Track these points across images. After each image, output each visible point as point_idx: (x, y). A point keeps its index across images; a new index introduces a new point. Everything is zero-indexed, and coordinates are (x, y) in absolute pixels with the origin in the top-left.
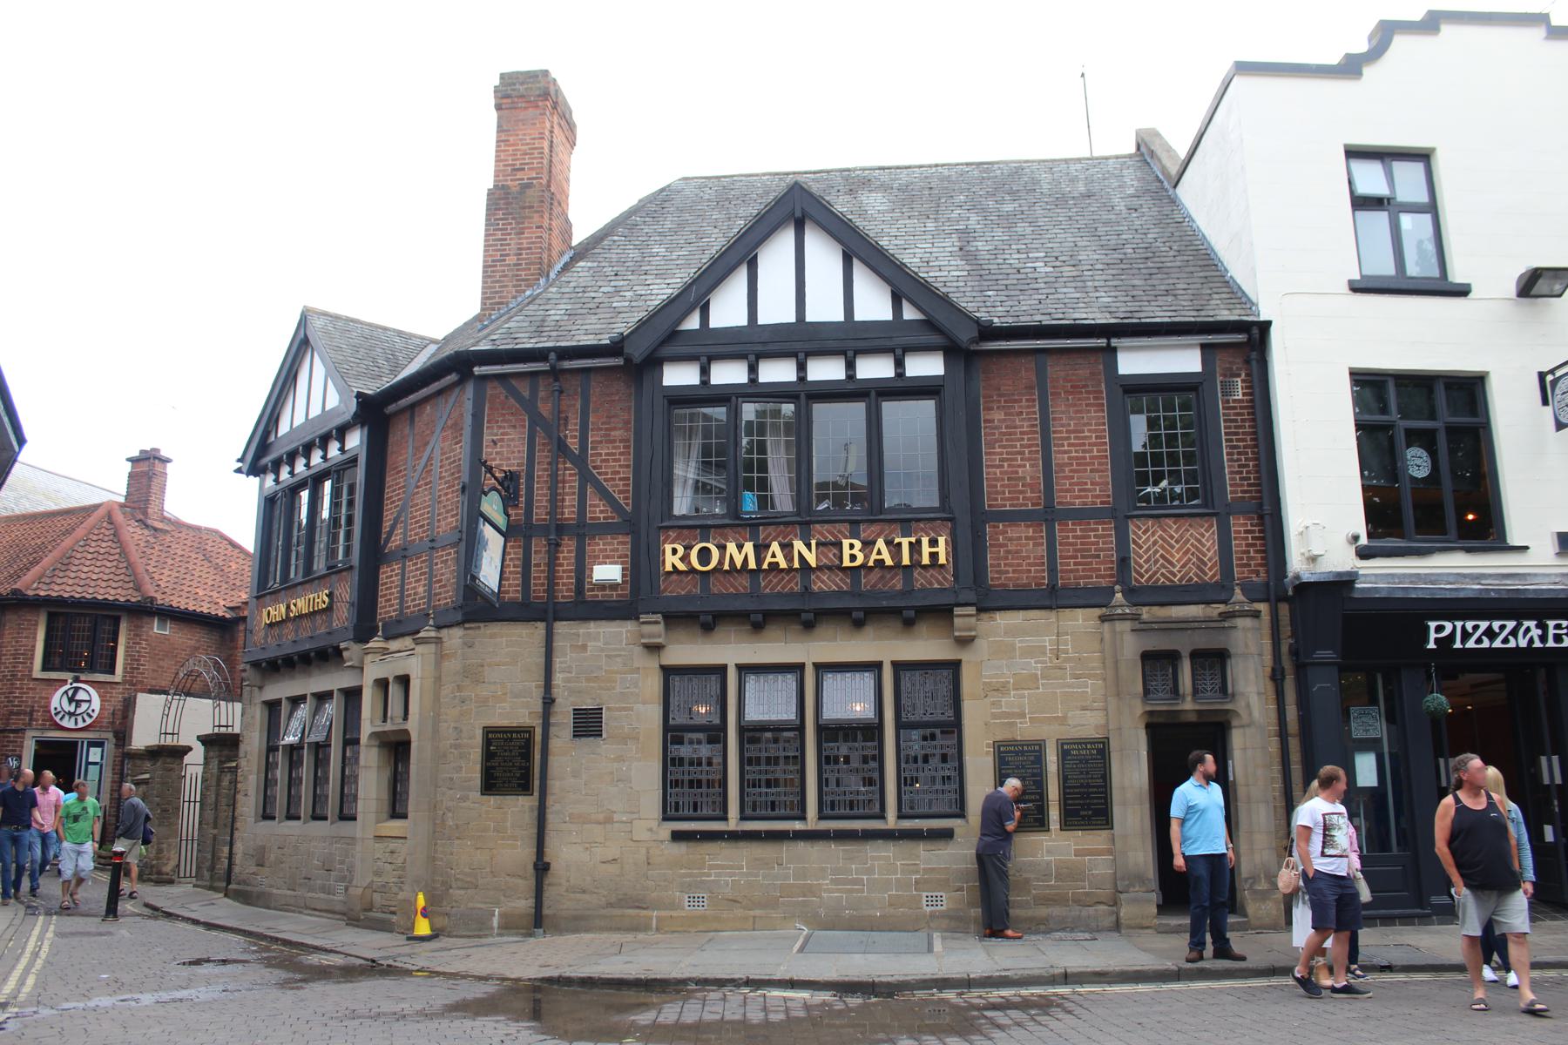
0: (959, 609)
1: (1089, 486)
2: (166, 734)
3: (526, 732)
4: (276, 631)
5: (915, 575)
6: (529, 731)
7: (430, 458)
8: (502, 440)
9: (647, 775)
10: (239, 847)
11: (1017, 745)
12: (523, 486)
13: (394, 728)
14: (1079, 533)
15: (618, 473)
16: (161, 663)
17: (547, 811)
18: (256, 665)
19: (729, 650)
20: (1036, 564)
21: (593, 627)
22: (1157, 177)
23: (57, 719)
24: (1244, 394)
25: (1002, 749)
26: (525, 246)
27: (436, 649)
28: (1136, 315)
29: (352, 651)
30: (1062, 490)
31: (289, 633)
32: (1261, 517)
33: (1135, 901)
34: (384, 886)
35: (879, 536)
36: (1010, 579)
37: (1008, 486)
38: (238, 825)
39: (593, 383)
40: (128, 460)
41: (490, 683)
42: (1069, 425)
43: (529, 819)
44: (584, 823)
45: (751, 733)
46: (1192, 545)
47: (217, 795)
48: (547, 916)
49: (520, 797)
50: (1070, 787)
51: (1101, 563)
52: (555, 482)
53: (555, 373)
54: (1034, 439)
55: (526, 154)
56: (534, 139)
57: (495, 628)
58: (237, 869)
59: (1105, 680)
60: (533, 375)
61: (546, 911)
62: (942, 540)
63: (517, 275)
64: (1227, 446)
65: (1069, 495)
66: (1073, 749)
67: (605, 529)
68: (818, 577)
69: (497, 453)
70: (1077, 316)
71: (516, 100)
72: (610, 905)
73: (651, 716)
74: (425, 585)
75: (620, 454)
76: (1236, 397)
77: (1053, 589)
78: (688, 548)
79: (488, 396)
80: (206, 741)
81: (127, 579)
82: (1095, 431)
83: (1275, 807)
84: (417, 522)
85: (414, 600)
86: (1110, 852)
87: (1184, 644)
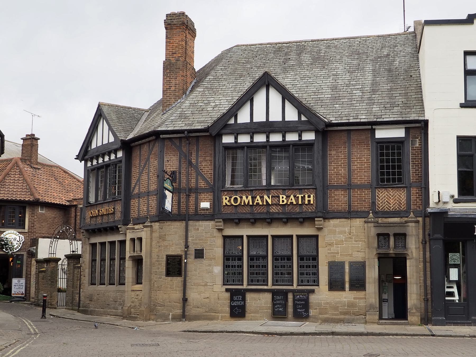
0: (317, 218)
2: (51, 254)
3: (180, 256)
4: (94, 219)
6: (181, 256)
9: (218, 270)
11: (336, 263)
14: (359, 193)
17: (187, 282)
18: (87, 231)
20: (344, 203)
21: (201, 223)
24: (419, 145)
25: (331, 264)
27: (151, 229)
29: (122, 228)
31: (99, 220)
33: (370, 314)
34: (135, 306)
36: (335, 208)
37: (336, 177)
40: (22, 139)
41: (168, 241)
42: (358, 156)
44: (198, 286)
51: (366, 203)
52: (188, 174)
53: (187, 138)
55: (176, 47)
56: (179, 41)
57: (169, 223)
58: (81, 302)
60: (180, 138)
61: (186, 314)
63: (175, 94)
65: (356, 180)
67: (204, 191)
69: (169, 164)
72: (206, 312)
73: (219, 252)
74: (146, 207)
75: (209, 165)
77: (349, 212)
78: (230, 198)
80: (68, 257)
81: (27, 191)
82: (366, 158)
84: (143, 186)
87: (391, 231)
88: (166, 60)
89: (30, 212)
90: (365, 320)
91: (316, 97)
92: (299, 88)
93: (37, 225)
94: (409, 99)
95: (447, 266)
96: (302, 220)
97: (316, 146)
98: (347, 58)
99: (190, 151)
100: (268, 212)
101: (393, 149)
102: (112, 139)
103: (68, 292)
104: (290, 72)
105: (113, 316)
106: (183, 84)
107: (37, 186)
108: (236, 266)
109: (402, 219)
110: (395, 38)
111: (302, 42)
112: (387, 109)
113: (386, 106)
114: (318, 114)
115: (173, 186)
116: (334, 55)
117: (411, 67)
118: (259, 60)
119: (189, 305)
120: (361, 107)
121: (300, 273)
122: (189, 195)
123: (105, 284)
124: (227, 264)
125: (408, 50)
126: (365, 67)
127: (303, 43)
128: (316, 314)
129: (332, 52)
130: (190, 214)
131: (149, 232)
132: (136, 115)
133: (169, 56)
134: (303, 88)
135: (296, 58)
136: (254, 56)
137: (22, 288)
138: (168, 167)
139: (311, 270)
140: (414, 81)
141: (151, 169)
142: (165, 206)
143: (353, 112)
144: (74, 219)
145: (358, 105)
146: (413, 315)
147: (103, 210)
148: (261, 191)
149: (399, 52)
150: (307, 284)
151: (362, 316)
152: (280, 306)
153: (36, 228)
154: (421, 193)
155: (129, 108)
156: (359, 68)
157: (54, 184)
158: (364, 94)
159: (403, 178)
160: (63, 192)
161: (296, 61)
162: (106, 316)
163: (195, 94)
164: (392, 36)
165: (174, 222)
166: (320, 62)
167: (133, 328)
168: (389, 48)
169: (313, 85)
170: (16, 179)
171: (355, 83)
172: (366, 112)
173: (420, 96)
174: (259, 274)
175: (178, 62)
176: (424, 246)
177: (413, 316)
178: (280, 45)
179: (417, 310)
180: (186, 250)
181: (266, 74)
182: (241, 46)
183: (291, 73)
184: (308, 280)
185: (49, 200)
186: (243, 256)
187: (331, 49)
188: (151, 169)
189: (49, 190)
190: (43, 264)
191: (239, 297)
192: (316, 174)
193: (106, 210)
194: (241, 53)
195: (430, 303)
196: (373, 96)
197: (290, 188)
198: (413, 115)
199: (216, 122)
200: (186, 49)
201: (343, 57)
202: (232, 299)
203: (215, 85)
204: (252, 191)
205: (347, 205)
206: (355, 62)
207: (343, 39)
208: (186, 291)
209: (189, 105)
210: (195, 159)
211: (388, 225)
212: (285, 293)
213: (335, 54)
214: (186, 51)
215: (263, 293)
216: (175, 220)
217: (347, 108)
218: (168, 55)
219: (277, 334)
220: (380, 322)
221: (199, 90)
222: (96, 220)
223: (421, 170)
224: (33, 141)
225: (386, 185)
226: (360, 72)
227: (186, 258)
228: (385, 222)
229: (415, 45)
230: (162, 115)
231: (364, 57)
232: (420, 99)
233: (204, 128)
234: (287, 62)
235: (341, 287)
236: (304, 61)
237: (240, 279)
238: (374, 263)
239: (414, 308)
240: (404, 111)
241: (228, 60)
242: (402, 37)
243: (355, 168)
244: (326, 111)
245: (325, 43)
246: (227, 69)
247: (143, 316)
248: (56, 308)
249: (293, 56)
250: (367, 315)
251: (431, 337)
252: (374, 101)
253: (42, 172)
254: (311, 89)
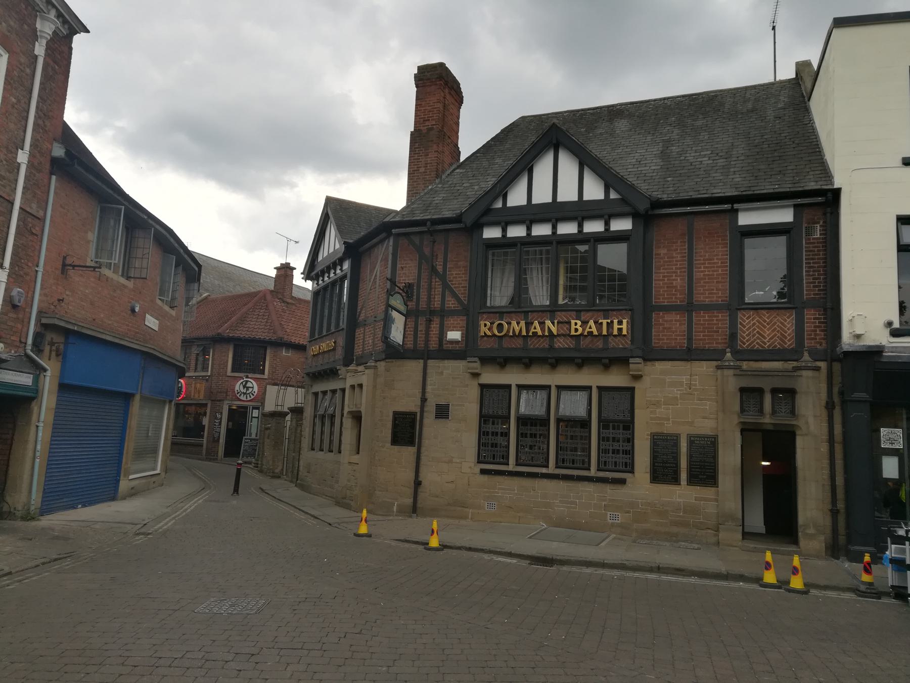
2: (281, 406)
3: (413, 415)
5: (610, 340)
6: (415, 414)
7: (376, 276)
8: (406, 267)
9: (470, 439)
10: (301, 463)
12: (415, 291)
14: (707, 318)
17: (422, 455)
19: (512, 377)
22: (803, 93)
23: (238, 395)
24: (820, 235)
26: (429, 162)
28: (753, 189)
29: (342, 370)
30: (698, 294)
32: (825, 310)
38: (301, 452)
40: (275, 268)
43: (413, 459)
45: (523, 421)
46: (778, 326)
47: (295, 437)
49: (409, 447)
50: (694, 462)
53: (431, 233)
55: (430, 111)
56: (434, 103)
58: (300, 473)
59: (717, 402)
61: (419, 505)
62: (625, 321)
63: (425, 178)
64: (806, 267)
65: (702, 296)
66: (697, 440)
67: (453, 313)
68: (558, 340)
70: (715, 191)
71: (425, 81)
73: (472, 410)
75: (463, 274)
77: (689, 349)
78: (492, 323)
83: (823, 485)
84: (370, 307)
85: (368, 346)
86: (716, 500)
87: (767, 384)
91: (636, 170)
133: (419, 124)
142: (391, 335)
146: (811, 537)
151: (709, 531)
170: (261, 314)
200: (444, 114)
210: (441, 265)
214: (444, 117)
237: (505, 454)
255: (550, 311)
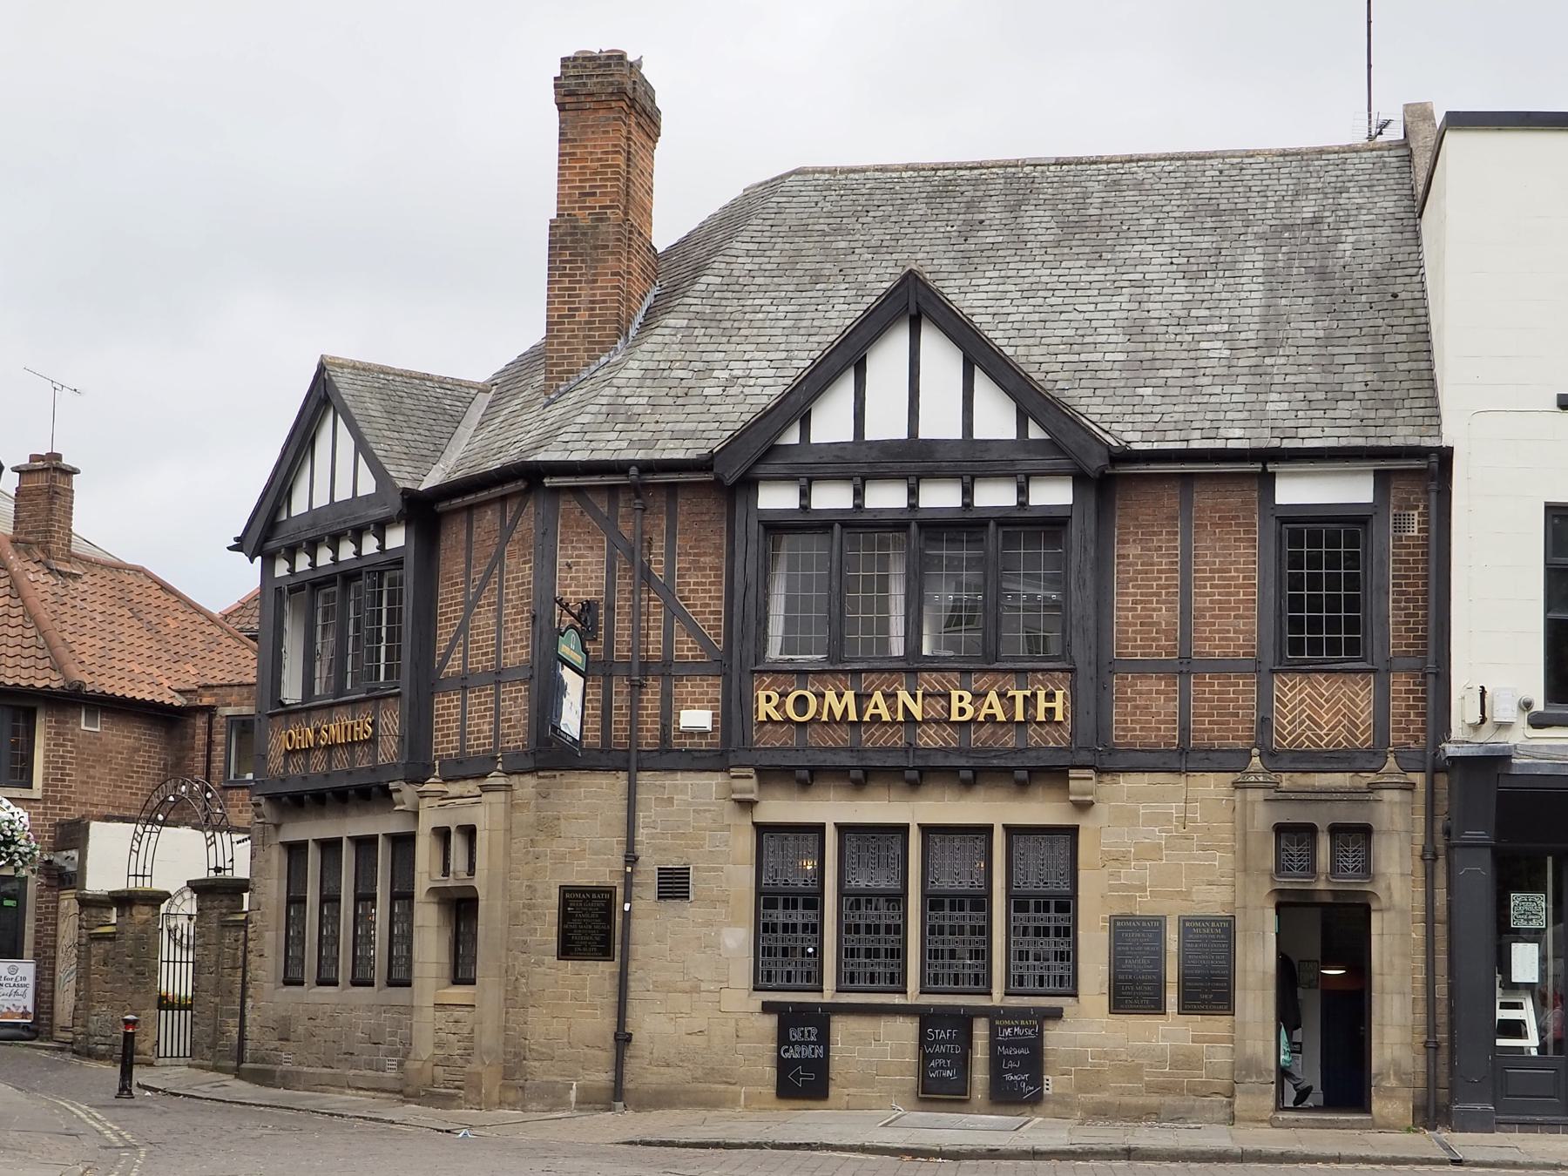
1: (1232, 635)
2: (136, 875)
6: (610, 891)
8: (577, 564)
9: (738, 939)
11: (1135, 921)
13: (458, 884)
14: (1216, 688)
15: (708, 605)
16: (92, 771)
17: (629, 977)
18: (273, 798)
20: (1165, 722)
21: (680, 779)
24: (1420, 530)
25: (1118, 924)
27: (506, 797)
29: (406, 793)
33: (1247, 1092)
35: (991, 687)
36: (1137, 737)
37: (1140, 632)
39: (679, 500)
42: (1214, 563)
43: (609, 987)
48: (628, 1090)
51: (1240, 722)
52: (637, 614)
53: (637, 490)
54: (1174, 578)
55: (596, 173)
56: (607, 153)
57: (572, 778)
58: (249, 1045)
60: (612, 489)
61: (628, 1085)
63: (589, 336)
65: (1209, 645)
67: (693, 669)
68: (924, 731)
73: (741, 879)
74: (490, 723)
76: (1411, 534)
77: (1183, 751)
78: (783, 695)
79: (561, 510)
81: (40, 654)
84: (479, 648)
87: (1321, 817)
88: (558, 215)
89: (49, 727)
90: (1228, 1110)
91: (1076, 358)
92: (1016, 325)
93: (75, 776)
94: (1388, 376)
95: (1505, 934)
96: (1023, 775)
97: (1075, 529)
98: (1178, 226)
99: (646, 533)
100: (910, 748)
101: (1333, 541)
102: (367, 486)
103: (198, 1008)
104: (984, 268)
105: (366, 1093)
106: (619, 301)
107: (72, 638)
108: (800, 928)
109: (1357, 779)
110: (1340, 161)
111: (1024, 164)
112: (1313, 405)
113: (1310, 396)
114: (1083, 419)
115: (587, 653)
116: (1135, 216)
117: (1393, 263)
118: (878, 225)
119: (636, 1057)
120: (1227, 398)
121: (764, 948)
122: (641, 686)
123: (336, 984)
124: (767, 920)
125: (1385, 204)
126: (1241, 258)
127: (1028, 169)
128: (1067, 1091)
129: (1126, 204)
130: (645, 748)
131: (500, 810)
132: (448, 402)
133: (569, 202)
134: (1029, 326)
135: (1003, 222)
136: (860, 208)
137: (24, 995)
138: (570, 586)
139: (1049, 945)
140: (1403, 313)
141: (507, 594)
142: (562, 722)
143: (1200, 416)
144: (203, 756)
145: (1218, 390)
146: (1390, 1094)
147: (336, 729)
148: (887, 675)
149: (1355, 212)
150: (1038, 988)
152: (946, 1064)
153: (71, 787)
154: (1424, 692)
155: (425, 378)
156: (1218, 263)
157: (131, 631)
158: (1238, 353)
159: (1365, 642)
160: (164, 659)
161: (1005, 232)
162: (340, 1093)
163: (660, 338)
164: (1329, 153)
165: (588, 776)
166: (1085, 236)
167: (448, 1131)
168: (1321, 196)
169: (1063, 316)
171: (1207, 313)
172: (1245, 415)
173: (1423, 365)
174: (877, 953)
175: (603, 227)
176: (1429, 870)
177: (1390, 1098)
178: (947, 172)
179: (1401, 1080)
180: (629, 869)
181: (911, 280)
182: (814, 172)
183: (988, 275)
184: (1041, 977)
185: (117, 686)
186: (822, 894)
187: (1124, 194)
188: (507, 594)
189: (112, 654)
190: (104, 910)
191: (809, 1031)
192: (1074, 623)
193: (346, 728)
194: (816, 199)
195: (1443, 1056)
196: (1268, 361)
197: (986, 666)
198: (1402, 431)
199: (736, 439)
201: (1165, 221)
202: (783, 1039)
203: (728, 309)
204: (856, 673)
205: (1175, 728)
206: (1205, 242)
207: (1165, 159)
208: (629, 1008)
209: (640, 374)
211: (1313, 796)
212: (962, 1021)
213: (1136, 210)
214: (628, 186)
215: (890, 1019)
216: (592, 769)
217: (1181, 399)
218: (566, 200)
219: (942, 1154)
220: (1280, 1117)
221: (672, 322)
222: (308, 763)
223: (1425, 615)
224: (55, 477)
225: (1307, 662)
226: (1223, 277)
227: (628, 898)
228: (1299, 786)
229: (1406, 187)
230: (545, 407)
231: (1234, 224)
232: (1426, 375)
233: (695, 457)
234: (974, 233)
235: (1151, 1002)
236: (1031, 232)
238: (1264, 922)
239: (1391, 1072)
240: (1372, 414)
241: (770, 222)
242: (1363, 161)
243: (1205, 603)
244: (1109, 409)
245: (1101, 172)
246: (768, 253)
247: (480, 1092)
248: (151, 1064)
249: (993, 212)
250: (1237, 1094)
251: (1451, 1168)
252: (1272, 378)
253: (85, 587)
254: (1057, 332)
255: (907, 671)
